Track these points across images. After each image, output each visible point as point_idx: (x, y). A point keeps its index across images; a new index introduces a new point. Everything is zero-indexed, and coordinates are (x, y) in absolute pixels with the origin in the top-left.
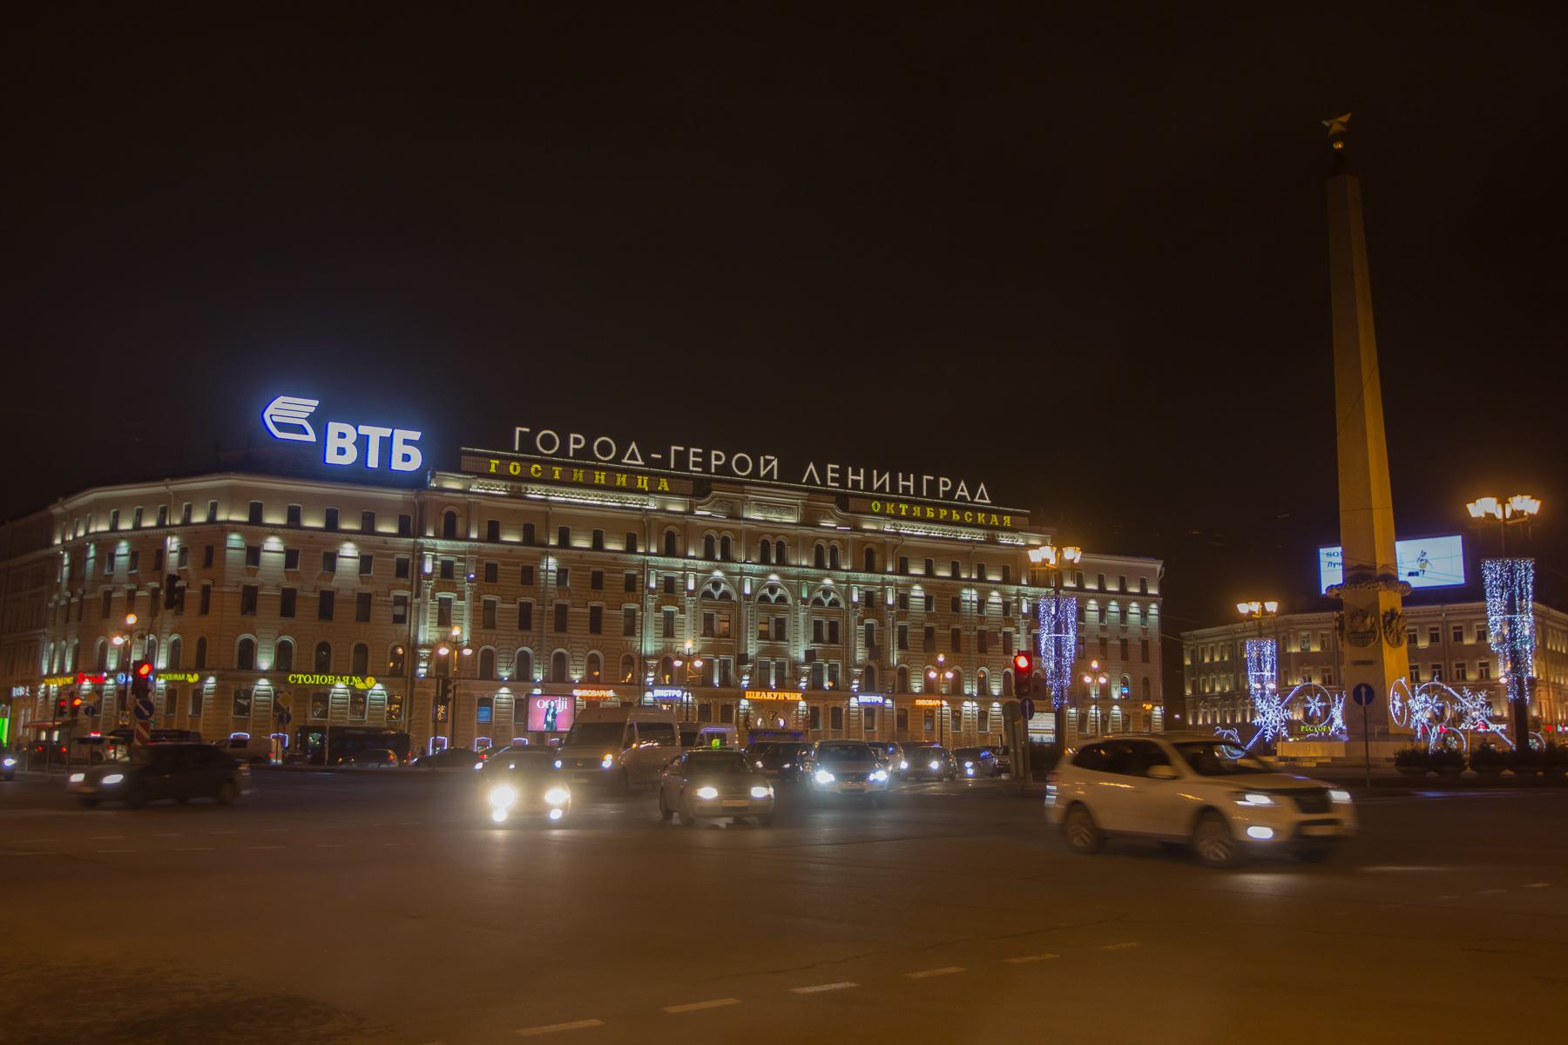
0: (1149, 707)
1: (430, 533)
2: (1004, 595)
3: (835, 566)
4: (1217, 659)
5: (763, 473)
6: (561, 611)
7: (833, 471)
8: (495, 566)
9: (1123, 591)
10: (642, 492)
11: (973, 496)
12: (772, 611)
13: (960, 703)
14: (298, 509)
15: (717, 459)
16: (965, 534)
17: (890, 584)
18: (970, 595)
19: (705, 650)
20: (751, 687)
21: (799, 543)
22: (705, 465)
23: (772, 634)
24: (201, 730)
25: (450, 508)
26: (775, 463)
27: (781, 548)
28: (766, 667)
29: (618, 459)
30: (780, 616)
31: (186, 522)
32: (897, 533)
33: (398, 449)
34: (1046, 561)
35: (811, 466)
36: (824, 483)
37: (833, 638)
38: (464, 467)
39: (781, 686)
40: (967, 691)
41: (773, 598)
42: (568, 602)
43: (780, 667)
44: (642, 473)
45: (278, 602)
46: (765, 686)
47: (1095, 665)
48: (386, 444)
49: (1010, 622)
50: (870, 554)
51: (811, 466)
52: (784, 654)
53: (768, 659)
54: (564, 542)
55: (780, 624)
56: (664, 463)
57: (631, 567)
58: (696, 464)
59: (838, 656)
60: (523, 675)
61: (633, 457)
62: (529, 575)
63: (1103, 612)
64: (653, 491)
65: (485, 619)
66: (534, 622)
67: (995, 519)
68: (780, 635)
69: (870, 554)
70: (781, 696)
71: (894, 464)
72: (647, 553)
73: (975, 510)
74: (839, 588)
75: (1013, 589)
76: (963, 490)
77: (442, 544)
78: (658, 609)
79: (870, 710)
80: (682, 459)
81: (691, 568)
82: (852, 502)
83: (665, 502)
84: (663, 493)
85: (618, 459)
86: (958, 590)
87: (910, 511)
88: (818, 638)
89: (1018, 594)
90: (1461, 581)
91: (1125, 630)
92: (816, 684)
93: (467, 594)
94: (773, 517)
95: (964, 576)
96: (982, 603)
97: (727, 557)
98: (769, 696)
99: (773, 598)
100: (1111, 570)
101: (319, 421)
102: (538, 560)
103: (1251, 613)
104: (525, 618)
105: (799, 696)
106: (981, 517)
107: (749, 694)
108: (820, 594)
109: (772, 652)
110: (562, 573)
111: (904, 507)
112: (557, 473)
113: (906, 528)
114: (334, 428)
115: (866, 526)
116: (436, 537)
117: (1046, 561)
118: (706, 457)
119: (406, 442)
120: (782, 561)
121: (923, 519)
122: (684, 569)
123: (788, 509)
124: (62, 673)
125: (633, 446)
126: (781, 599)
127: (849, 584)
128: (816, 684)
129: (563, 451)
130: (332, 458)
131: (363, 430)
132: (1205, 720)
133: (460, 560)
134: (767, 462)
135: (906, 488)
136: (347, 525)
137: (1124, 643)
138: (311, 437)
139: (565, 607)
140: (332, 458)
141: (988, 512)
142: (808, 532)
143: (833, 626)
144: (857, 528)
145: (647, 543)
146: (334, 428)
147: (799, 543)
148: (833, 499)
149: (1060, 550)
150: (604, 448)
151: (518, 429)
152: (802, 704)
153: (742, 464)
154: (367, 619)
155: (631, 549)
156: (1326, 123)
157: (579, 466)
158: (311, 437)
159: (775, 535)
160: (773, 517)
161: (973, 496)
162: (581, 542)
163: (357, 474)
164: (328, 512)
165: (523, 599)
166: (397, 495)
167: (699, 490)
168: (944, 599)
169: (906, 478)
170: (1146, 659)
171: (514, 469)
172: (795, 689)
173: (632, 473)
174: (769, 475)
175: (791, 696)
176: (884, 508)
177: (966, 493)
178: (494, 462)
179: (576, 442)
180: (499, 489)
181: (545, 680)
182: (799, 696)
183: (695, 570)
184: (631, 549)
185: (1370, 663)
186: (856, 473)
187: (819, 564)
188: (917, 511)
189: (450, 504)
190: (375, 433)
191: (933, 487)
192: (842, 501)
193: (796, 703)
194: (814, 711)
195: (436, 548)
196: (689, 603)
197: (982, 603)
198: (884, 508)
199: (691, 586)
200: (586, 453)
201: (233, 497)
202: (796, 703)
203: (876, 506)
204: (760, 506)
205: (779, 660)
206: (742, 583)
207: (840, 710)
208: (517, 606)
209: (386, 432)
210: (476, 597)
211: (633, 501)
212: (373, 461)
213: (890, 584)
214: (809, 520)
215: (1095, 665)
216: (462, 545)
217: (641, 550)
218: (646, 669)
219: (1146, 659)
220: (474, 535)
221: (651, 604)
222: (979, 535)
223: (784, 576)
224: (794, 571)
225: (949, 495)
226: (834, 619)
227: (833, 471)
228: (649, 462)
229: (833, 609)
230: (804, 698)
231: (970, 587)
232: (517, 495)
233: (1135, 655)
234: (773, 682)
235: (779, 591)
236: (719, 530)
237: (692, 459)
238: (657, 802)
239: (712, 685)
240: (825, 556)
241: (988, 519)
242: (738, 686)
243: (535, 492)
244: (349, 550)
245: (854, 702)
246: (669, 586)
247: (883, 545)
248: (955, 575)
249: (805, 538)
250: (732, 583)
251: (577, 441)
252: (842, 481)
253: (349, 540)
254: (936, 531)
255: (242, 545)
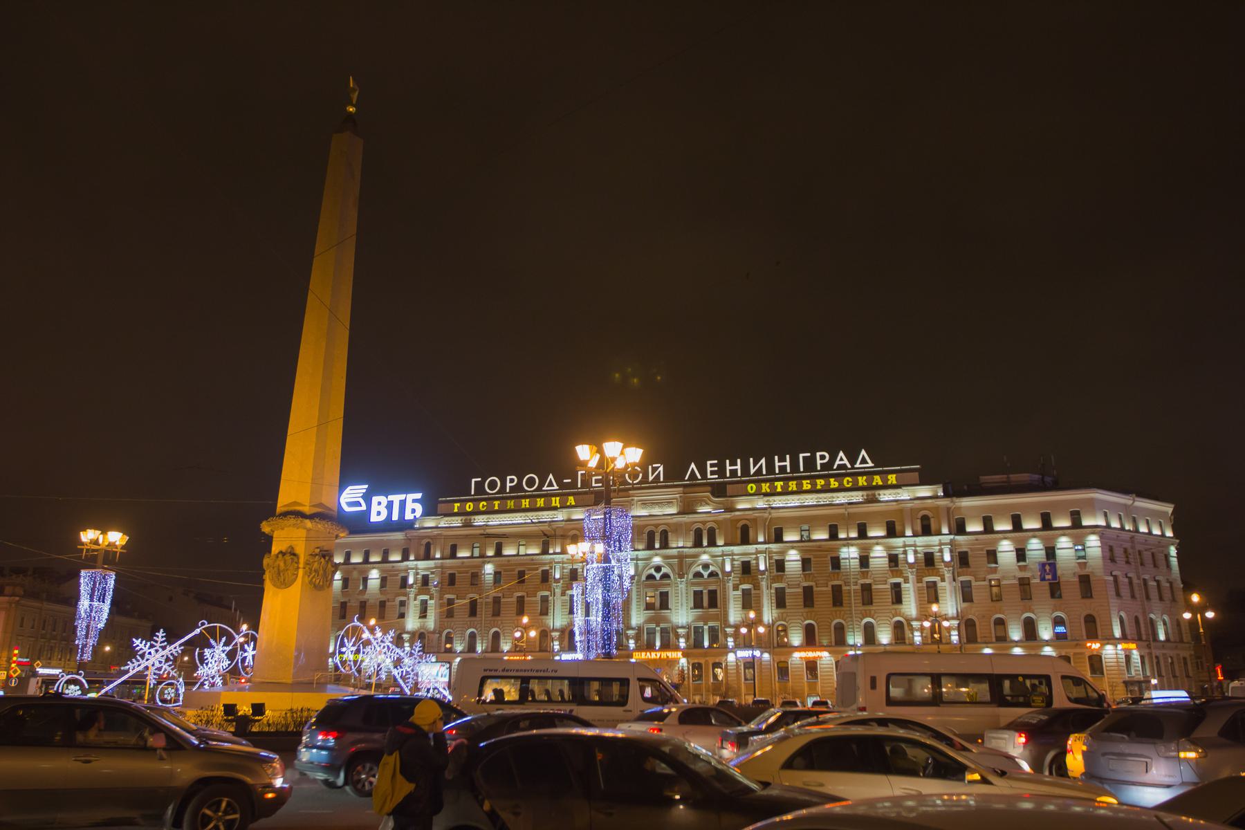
0: (1096, 646)
1: (909, 532)
2: (888, 548)
3: (712, 543)
5: (651, 478)
7: (712, 466)
10: (555, 508)
11: (853, 462)
12: (656, 587)
14: (836, 526)
16: (841, 498)
17: (761, 552)
18: (850, 554)
21: (678, 529)
23: (658, 605)
26: (661, 469)
28: (651, 633)
29: (540, 488)
30: (665, 590)
32: (570, 520)
33: (410, 506)
35: (693, 466)
37: (713, 603)
39: (666, 646)
40: (850, 641)
41: (658, 576)
42: (868, 581)
43: (663, 631)
46: (650, 647)
48: (403, 504)
49: (899, 574)
51: (693, 466)
52: (666, 620)
53: (653, 626)
55: (664, 597)
56: (573, 485)
57: (545, 564)
58: (712, 473)
59: (715, 618)
61: (551, 484)
62: (476, 577)
63: (1021, 554)
64: (564, 506)
65: (448, 612)
67: (878, 480)
68: (664, 604)
70: (664, 655)
74: (716, 562)
75: (898, 542)
76: (842, 459)
77: (422, 564)
79: (750, 664)
83: (570, 513)
86: (837, 549)
87: (785, 487)
88: (698, 604)
93: (911, 577)
94: (656, 511)
96: (864, 561)
98: (654, 655)
101: (367, 497)
102: (481, 566)
104: (473, 609)
105: (680, 654)
106: (862, 481)
109: (657, 620)
110: (497, 574)
111: (779, 484)
113: (778, 502)
114: (375, 499)
115: (740, 506)
119: (414, 501)
120: (665, 545)
122: (723, 555)
123: (669, 503)
125: (863, 452)
127: (724, 557)
130: (374, 518)
131: (391, 498)
134: (654, 470)
136: (1057, 523)
138: (364, 507)
140: (374, 518)
141: (869, 474)
143: (713, 594)
144: (730, 509)
146: (375, 499)
147: (678, 529)
148: (709, 488)
150: (531, 483)
151: (801, 455)
152: (683, 661)
153: (493, 485)
158: (364, 507)
160: (656, 511)
161: (853, 462)
163: (388, 526)
165: (471, 595)
166: (399, 536)
168: (822, 560)
169: (782, 459)
171: (469, 507)
172: (677, 648)
173: (548, 496)
175: (672, 655)
176: (799, 485)
177: (846, 461)
178: (457, 505)
180: (457, 522)
181: (688, 647)
182: (680, 654)
183: (733, 554)
189: (925, 509)
190: (396, 499)
191: (810, 463)
192: (719, 490)
193: (676, 661)
195: (416, 568)
197: (864, 561)
198: (759, 488)
200: (518, 487)
202: (676, 661)
203: (752, 488)
204: (645, 504)
205: (663, 625)
208: (830, 588)
209: (402, 497)
211: (546, 516)
212: (395, 517)
213: (761, 552)
214: (687, 509)
216: (431, 563)
217: (551, 551)
221: (558, 591)
222: (857, 497)
223: (666, 557)
224: (674, 552)
226: (712, 588)
229: (712, 579)
230: (684, 656)
231: (848, 545)
232: (467, 525)
234: (658, 644)
237: (709, 469)
240: (703, 537)
241: (870, 481)
243: (479, 520)
244: (374, 574)
245: (731, 657)
247: (755, 520)
248: (834, 536)
251: (822, 457)
252: (721, 472)
253: (1034, 537)
254: (810, 500)
255: (798, 558)
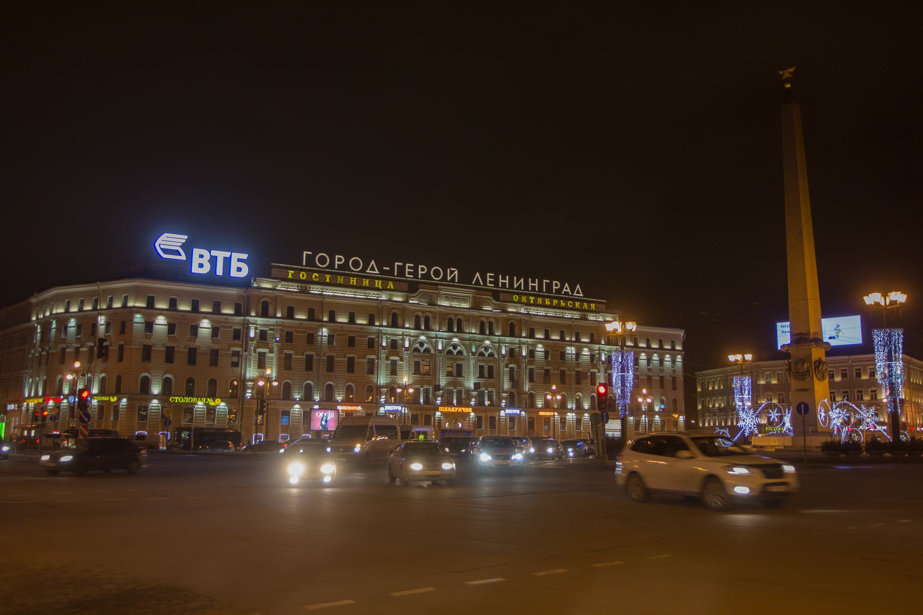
0: (676, 416)
1: (253, 314)
2: (591, 350)
3: (492, 333)
4: (716, 388)
5: (449, 278)
6: (330, 359)
7: (490, 277)
8: (292, 333)
9: (661, 348)
10: (378, 289)
11: (573, 292)
12: (455, 360)
13: (565, 414)
14: (175, 300)
15: (422, 270)
16: (568, 314)
17: (524, 343)
18: (571, 350)
19: (415, 382)
20: (442, 405)
21: (470, 320)
22: (415, 274)
23: (455, 373)
24: (118, 430)
25: (265, 299)
26: (456, 272)
27: (459, 322)
28: (451, 393)
29: (364, 270)
30: (459, 363)
31: (110, 307)
32: (528, 314)
33: (234, 264)
34: (616, 330)
35: (478, 274)
36: (485, 284)
37: (491, 375)
38: (273, 275)
39: (460, 404)
40: (569, 407)
41: (455, 352)
42: (334, 354)
43: (459, 392)
44: (378, 279)
45: (164, 354)
46: (450, 404)
47: (644, 391)
48: (227, 261)
49: (595, 366)
50: (512, 326)
51: (478, 274)
52: (462, 385)
53: (452, 388)
54: (332, 319)
55: (459, 368)
56: (391, 272)
57: (372, 333)
58: (410, 273)
59: (493, 386)
60: (308, 397)
61: (372, 269)
62: (311, 338)
63: (649, 360)
64: (385, 289)
65: (286, 364)
66: (314, 366)
67: (585, 305)
68: (459, 374)
69: (512, 326)
70: (460, 409)
71: (526, 273)
72: (381, 326)
73: (574, 300)
74: (494, 346)
75: (596, 347)
76: (567, 288)
77: (260, 320)
78: (387, 359)
79: (512, 418)
80: (402, 270)
81: (407, 334)
82: (501, 295)
83: (391, 296)
84: (390, 290)
85: (364, 270)
86: (564, 347)
87: (536, 301)
88: (481, 375)
89: (599, 350)
90: (860, 342)
91: (662, 370)
92: (480, 403)
93: (275, 349)
94: (455, 304)
95: (568, 339)
96: (578, 355)
97: (428, 328)
98: (453, 410)
99: (455, 352)
100: (654, 335)
101: (188, 248)
102: (317, 329)
103: (737, 361)
104: (309, 364)
105: (470, 410)
106: (577, 304)
107: (441, 409)
108: (483, 350)
109: (455, 384)
110: (331, 337)
111: (532, 298)
112: (328, 278)
113: (533, 311)
114: (197, 252)
115: (510, 310)
116: (257, 316)
117: (616, 330)
118: (416, 269)
119: (239, 260)
120: (460, 330)
121: (543, 306)
122: (403, 335)
123: (464, 299)
124: (36, 396)
125: (373, 262)
126: (460, 353)
127: (499, 344)
128: (480, 403)
129: (332, 265)
130: (195, 269)
131: (214, 253)
132: (709, 423)
133: (271, 330)
134: (452, 272)
135: (533, 287)
136: (204, 309)
137: (662, 378)
138: (183, 257)
139: (333, 357)
140: (195, 269)
141: (582, 301)
142: (476, 313)
143: (491, 369)
144: (504, 311)
145: (381, 320)
146: (197, 252)
147: (470, 320)
148: (490, 293)
149: (624, 324)
150: (356, 264)
151: (305, 253)
152: (472, 414)
153: (437, 273)
154: (216, 364)
155: (371, 323)
156: (781, 73)
157: (341, 274)
158: (183, 257)
159: (456, 315)
160: (455, 304)
161: (573, 292)
162: (342, 319)
163: (210, 279)
164: (193, 301)
165: (308, 353)
166: (234, 291)
167: (412, 288)
168: (556, 353)
169: (533, 282)
170: (674, 388)
171: (303, 276)
172: (468, 406)
173: (372, 278)
174: (453, 280)
175: (466, 410)
176: (520, 299)
177: (569, 290)
178: (291, 272)
179: (339, 260)
180: (294, 288)
181: (321, 400)
182: (470, 410)
183: (409, 335)
184: (371, 323)
185: (806, 390)
186: (504, 278)
187: (482, 332)
188: (540, 301)
189: (265, 297)
190: (221, 255)
191: (549, 286)
192: (496, 295)
193: (468, 414)
194: (479, 419)
195: (257, 323)
196: (406, 355)
197: (578, 355)
198: (520, 299)
199: (407, 345)
200: (345, 267)
201: (137, 293)
202: (468, 414)
203: (516, 298)
204: (448, 298)
205: (459, 388)
206: (436, 343)
207: (495, 418)
208: (304, 357)
209: (227, 254)
210: (280, 351)
211: (373, 295)
212: (220, 272)
213: (524, 343)
214: (476, 306)
215: (644, 391)
216: (272, 321)
217: (377, 324)
218: (380, 394)
219: (674, 388)
220: (279, 315)
221: (383, 356)
222: (576, 315)
223: (461, 339)
224: (467, 336)
225: (559, 291)
226: (491, 364)
227: (490, 277)
228: (382, 272)
229: (490, 358)
230: (473, 411)
231: (571, 346)
232: (304, 291)
233: (668, 385)
234: (455, 402)
235: (459, 348)
236: (423, 312)
237: (407, 270)
238: (387, 472)
239: (419, 403)
240: (486, 328)
241: (581, 305)
242: (434, 404)
243: (315, 290)
244: (205, 323)
245: (502, 413)
246: (394, 345)
247: (520, 321)
248: (562, 339)
249: (474, 317)
250: (431, 343)
251: (340, 260)
252: (496, 283)
253: (205, 318)
254: (551, 312)
255: (143, 321)
